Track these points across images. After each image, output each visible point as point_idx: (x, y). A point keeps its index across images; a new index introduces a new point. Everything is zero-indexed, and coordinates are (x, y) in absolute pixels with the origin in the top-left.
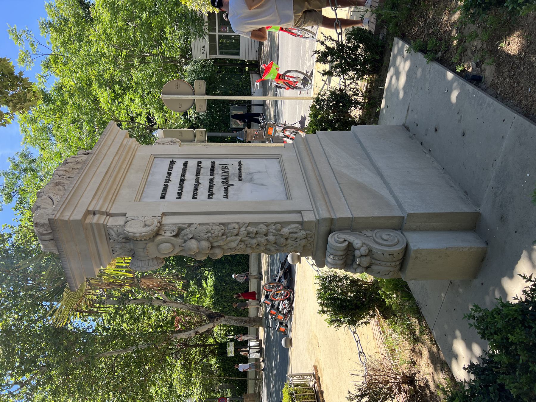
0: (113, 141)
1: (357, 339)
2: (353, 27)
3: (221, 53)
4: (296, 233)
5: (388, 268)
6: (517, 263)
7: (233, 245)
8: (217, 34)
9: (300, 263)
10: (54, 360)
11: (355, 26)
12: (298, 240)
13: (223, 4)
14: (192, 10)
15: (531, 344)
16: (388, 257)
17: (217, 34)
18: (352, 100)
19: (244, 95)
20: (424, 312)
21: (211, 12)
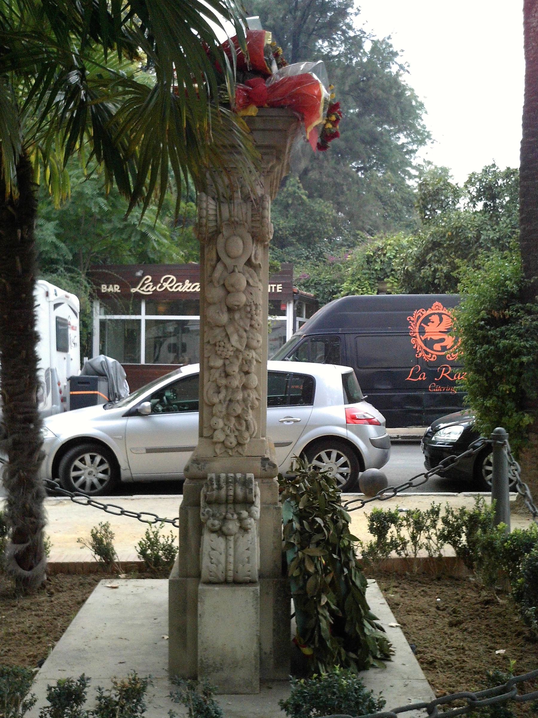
0: (263, 130)
1: (143, 517)
2: (124, 98)
3: (103, 323)
4: (247, 428)
5: (222, 559)
6: (525, 102)
7: (234, 339)
8: (143, 317)
9: (84, 674)
10: (525, 711)
11: (27, 415)
12: (237, 433)
13: (66, 320)
14: (368, 695)
15: (6, 316)
16: (245, 556)
17: (143, 317)
18: (463, 401)
19: (123, 314)
20: (290, 465)
21: (396, 59)
